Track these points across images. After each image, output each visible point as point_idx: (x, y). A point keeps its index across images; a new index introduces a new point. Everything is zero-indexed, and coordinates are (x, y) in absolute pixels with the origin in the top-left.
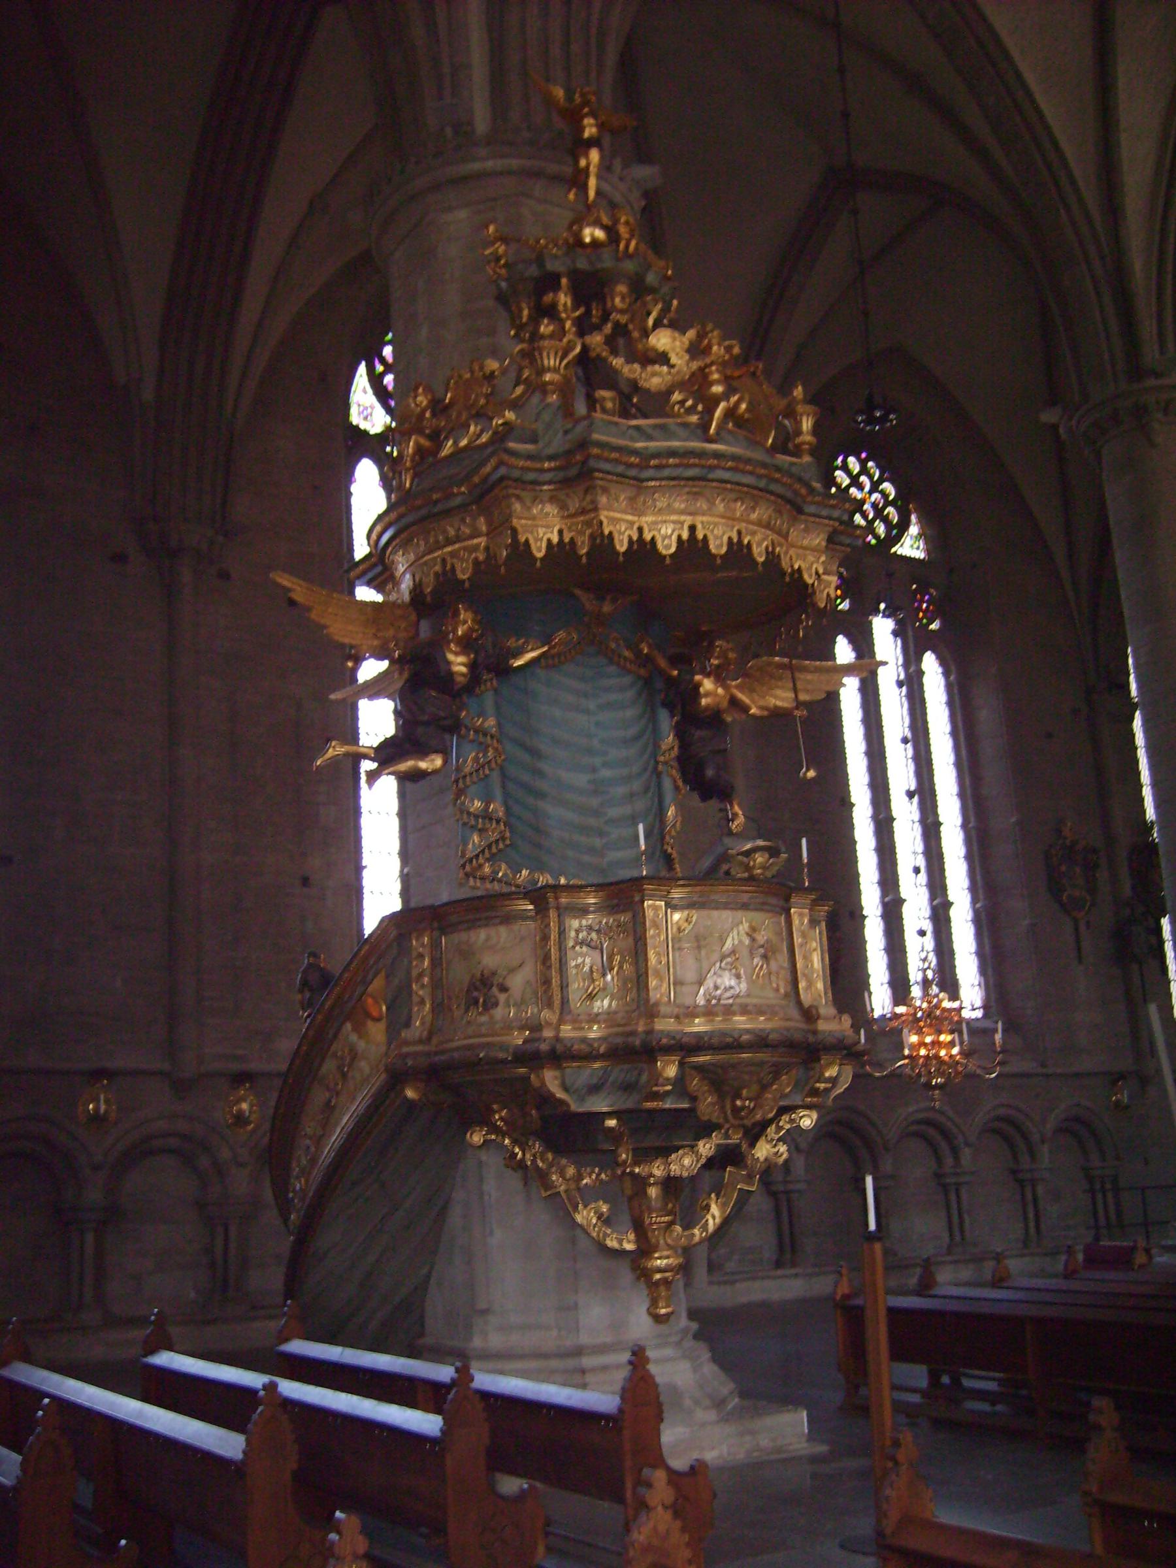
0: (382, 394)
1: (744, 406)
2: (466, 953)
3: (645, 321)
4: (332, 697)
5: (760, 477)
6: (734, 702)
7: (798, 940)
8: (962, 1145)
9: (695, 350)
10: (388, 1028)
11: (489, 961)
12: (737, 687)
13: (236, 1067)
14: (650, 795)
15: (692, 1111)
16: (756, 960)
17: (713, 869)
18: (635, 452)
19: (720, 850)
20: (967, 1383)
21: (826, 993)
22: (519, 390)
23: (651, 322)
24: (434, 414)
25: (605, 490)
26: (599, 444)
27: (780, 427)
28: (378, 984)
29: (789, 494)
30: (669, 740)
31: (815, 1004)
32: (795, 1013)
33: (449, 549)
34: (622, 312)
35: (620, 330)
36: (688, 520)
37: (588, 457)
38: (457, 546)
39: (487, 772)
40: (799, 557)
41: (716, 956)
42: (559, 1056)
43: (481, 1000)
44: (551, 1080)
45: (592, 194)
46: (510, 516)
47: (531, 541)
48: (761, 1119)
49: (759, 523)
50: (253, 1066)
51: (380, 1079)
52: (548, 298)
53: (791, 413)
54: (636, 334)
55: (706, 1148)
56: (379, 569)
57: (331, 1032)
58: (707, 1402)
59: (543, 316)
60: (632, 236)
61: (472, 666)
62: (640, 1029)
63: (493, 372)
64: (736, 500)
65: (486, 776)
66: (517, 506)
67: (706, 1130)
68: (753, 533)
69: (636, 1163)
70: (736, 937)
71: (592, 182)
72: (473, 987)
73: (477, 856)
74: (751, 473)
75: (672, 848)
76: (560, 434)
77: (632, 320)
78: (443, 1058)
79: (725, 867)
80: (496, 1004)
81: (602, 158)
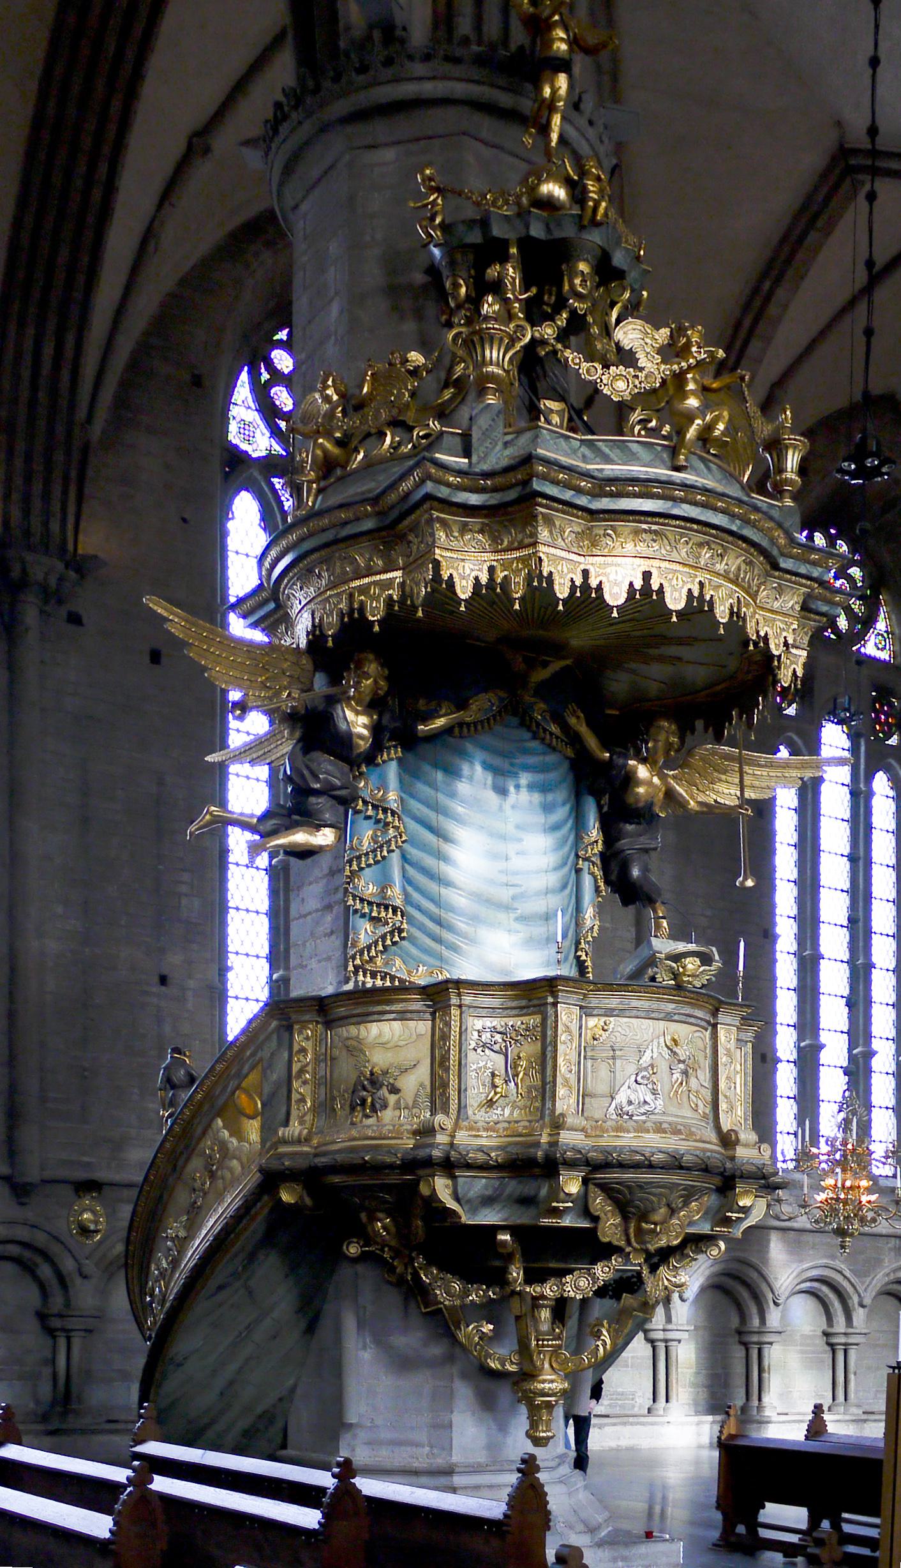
0: (269, 411)
1: (721, 426)
2: (355, 1049)
3: (608, 314)
4: (208, 759)
5: (733, 516)
6: (670, 794)
7: (723, 1059)
8: (856, 1306)
9: (672, 351)
10: (263, 1127)
11: (379, 1059)
12: (674, 777)
13: (81, 1175)
14: (568, 891)
15: (593, 1232)
16: (675, 1076)
17: (637, 974)
18: (587, 475)
19: (644, 953)
20: (847, 1528)
21: (745, 1120)
22: (447, 394)
23: (614, 315)
24: (344, 411)
25: (549, 521)
26: (547, 461)
27: (759, 462)
28: (253, 1078)
29: (765, 543)
30: (594, 833)
31: (735, 1128)
32: (713, 1136)
33: (357, 583)
34: (579, 297)
35: (577, 324)
36: (645, 565)
37: (531, 476)
38: (366, 580)
39: (385, 853)
40: (768, 622)
41: (631, 1069)
42: (449, 1166)
43: (369, 1100)
44: (442, 1187)
45: (554, 137)
46: (433, 545)
47: (456, 579)
48: (665, 1245)
49: (726, 576)
50: (101, 1175)
51: (250, 1180)
52: (493, 272)
53: (775, 446)
54: (595, 330)
55: (603, 1272)
56: (272, 605)
57: (199, 1131)
58: (581, 1527)
59: (487, 293)
60: (602, 198)
61: (376, 729)
62: (544, 1139)
63: (417, 368)
64: (700, 545)
65: (384, 858)
66: (441, 535)
67: (606, 1251)
68: (717, 588)
69: (528, 1281)
70: (655, 1050)
71: (557, 120)
72: (359, 1086)
73: (369, 948)
74: (723, 511)
75: (586, 956)
76: (500, 445)
77: (591, 311)
78: (323, 1160)
79: (650, 972)
80: (385, 1106)
81: (571, 86)
